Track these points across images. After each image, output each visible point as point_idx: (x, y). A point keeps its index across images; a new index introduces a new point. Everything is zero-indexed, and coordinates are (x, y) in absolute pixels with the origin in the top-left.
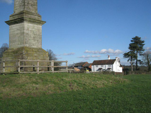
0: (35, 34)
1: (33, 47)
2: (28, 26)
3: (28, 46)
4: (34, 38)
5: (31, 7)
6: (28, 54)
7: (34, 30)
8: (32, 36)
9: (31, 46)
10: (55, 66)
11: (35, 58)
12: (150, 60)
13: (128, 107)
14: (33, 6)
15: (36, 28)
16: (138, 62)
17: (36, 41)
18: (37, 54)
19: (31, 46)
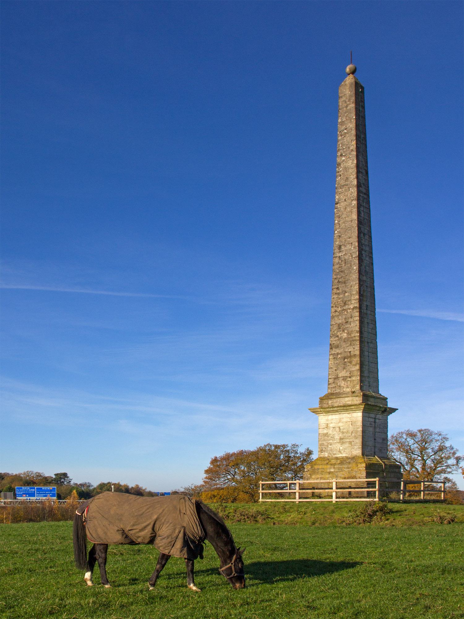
0: (343, 433)
1: (338, 456)
2: (327, 420)
3: (326, 455)
4: (341, 439)
5: (343, 383)
6: (314, 469)
7: (340, 424)
8: (337, 437)
9: (334, 454)
10: (301, 491)
11: (327, 476)
12: (233, 618)
13: (40, 537)
14: (349, 379)
15: (345, 420)
16: (325, 406)
17: (347, 445)
18: (334, 468)
19: (334, 454)
